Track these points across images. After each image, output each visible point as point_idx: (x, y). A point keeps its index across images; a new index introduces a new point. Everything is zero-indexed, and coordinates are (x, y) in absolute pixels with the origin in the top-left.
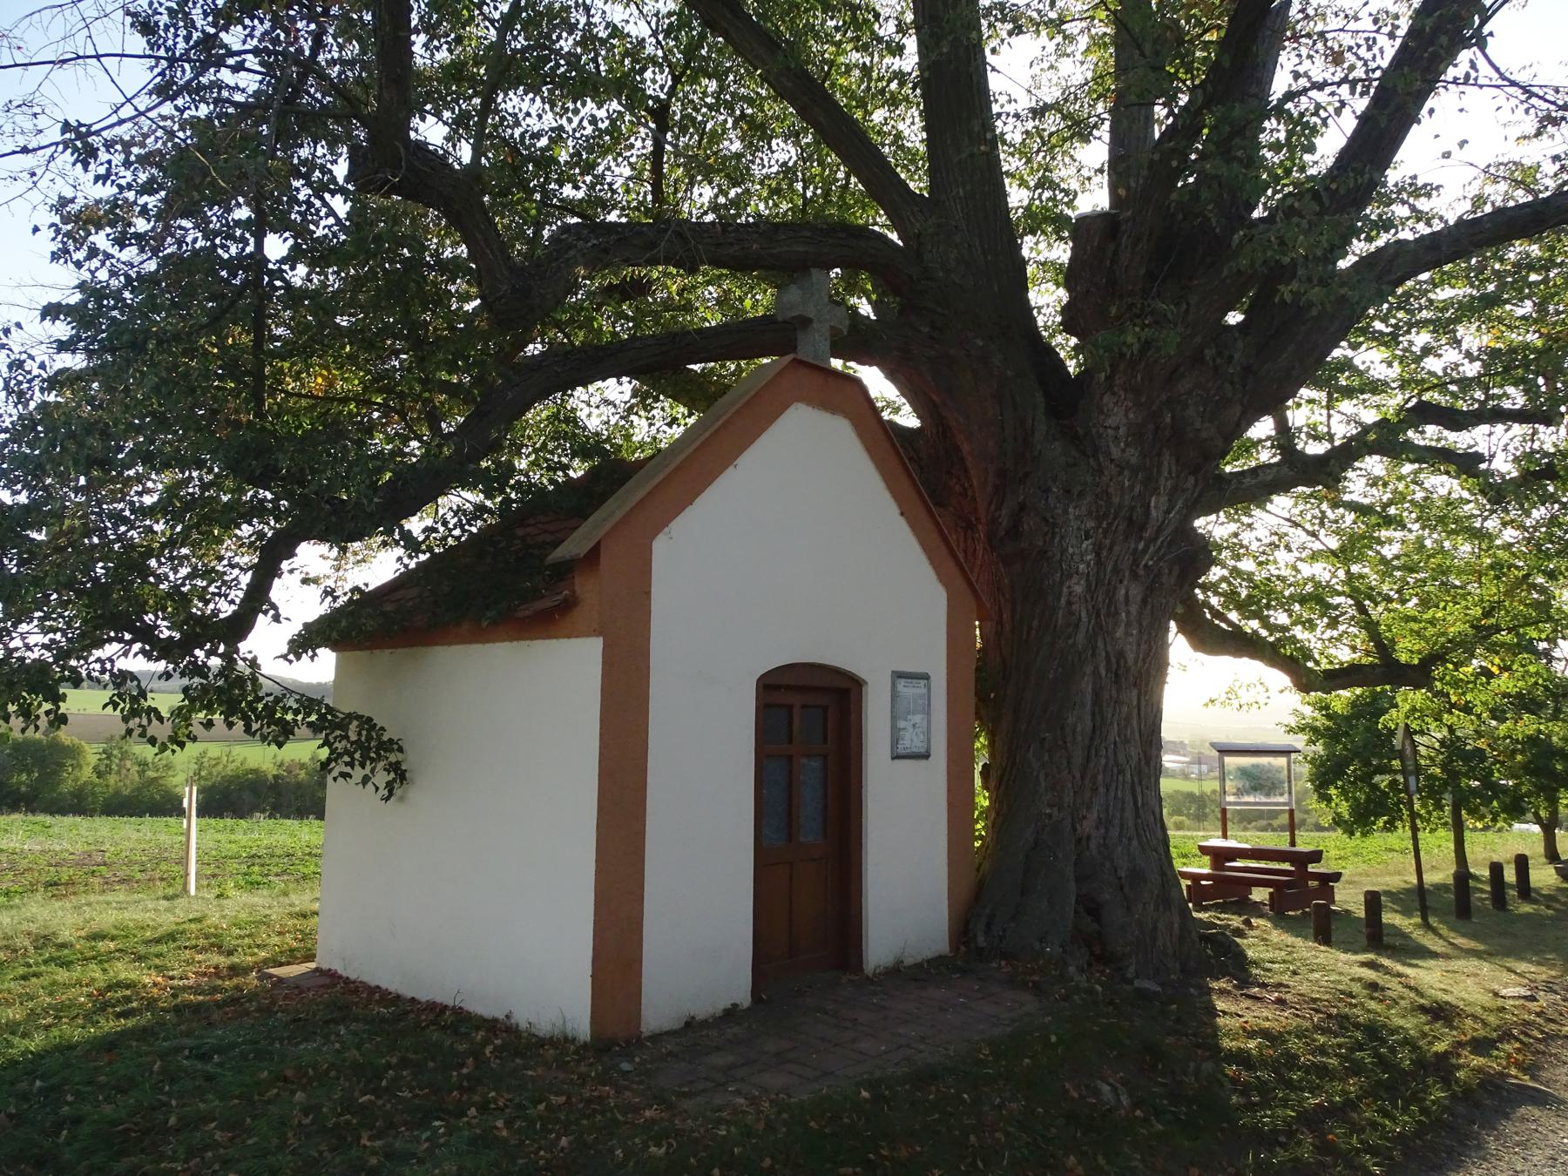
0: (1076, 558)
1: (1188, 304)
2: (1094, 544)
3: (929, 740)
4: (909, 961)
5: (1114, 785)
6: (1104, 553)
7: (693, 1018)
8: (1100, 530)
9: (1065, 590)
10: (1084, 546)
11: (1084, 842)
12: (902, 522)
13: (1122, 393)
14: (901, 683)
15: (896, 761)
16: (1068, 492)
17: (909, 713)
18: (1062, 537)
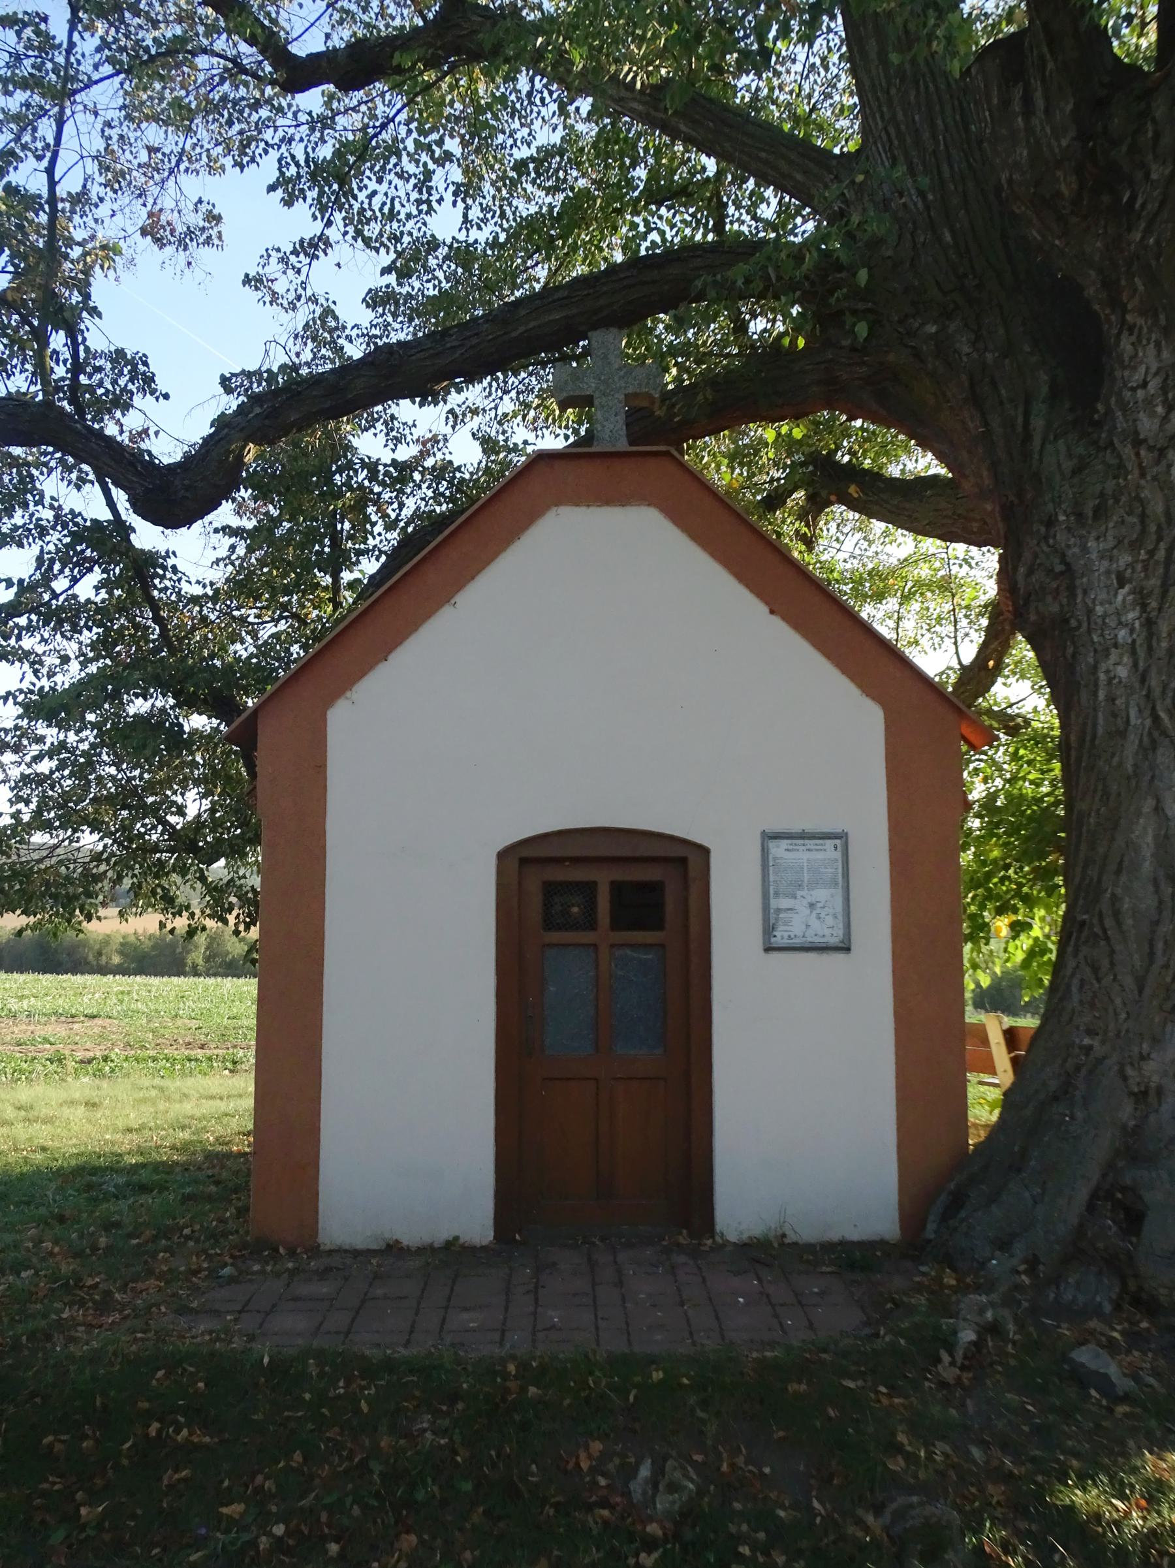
0: (1112, 622)
4: (791, 1238)
7: (397, 1241)
8: (1139, 567)
9: (1102, 676)
10: (1120, 598)
11: (1152, 1098)
12: (777, 622)
13: (1140, 321)
14: (779, 849)
15: (775, 955)
16: (1080, 516)
17: (800, 887)
18: (1085, 592)
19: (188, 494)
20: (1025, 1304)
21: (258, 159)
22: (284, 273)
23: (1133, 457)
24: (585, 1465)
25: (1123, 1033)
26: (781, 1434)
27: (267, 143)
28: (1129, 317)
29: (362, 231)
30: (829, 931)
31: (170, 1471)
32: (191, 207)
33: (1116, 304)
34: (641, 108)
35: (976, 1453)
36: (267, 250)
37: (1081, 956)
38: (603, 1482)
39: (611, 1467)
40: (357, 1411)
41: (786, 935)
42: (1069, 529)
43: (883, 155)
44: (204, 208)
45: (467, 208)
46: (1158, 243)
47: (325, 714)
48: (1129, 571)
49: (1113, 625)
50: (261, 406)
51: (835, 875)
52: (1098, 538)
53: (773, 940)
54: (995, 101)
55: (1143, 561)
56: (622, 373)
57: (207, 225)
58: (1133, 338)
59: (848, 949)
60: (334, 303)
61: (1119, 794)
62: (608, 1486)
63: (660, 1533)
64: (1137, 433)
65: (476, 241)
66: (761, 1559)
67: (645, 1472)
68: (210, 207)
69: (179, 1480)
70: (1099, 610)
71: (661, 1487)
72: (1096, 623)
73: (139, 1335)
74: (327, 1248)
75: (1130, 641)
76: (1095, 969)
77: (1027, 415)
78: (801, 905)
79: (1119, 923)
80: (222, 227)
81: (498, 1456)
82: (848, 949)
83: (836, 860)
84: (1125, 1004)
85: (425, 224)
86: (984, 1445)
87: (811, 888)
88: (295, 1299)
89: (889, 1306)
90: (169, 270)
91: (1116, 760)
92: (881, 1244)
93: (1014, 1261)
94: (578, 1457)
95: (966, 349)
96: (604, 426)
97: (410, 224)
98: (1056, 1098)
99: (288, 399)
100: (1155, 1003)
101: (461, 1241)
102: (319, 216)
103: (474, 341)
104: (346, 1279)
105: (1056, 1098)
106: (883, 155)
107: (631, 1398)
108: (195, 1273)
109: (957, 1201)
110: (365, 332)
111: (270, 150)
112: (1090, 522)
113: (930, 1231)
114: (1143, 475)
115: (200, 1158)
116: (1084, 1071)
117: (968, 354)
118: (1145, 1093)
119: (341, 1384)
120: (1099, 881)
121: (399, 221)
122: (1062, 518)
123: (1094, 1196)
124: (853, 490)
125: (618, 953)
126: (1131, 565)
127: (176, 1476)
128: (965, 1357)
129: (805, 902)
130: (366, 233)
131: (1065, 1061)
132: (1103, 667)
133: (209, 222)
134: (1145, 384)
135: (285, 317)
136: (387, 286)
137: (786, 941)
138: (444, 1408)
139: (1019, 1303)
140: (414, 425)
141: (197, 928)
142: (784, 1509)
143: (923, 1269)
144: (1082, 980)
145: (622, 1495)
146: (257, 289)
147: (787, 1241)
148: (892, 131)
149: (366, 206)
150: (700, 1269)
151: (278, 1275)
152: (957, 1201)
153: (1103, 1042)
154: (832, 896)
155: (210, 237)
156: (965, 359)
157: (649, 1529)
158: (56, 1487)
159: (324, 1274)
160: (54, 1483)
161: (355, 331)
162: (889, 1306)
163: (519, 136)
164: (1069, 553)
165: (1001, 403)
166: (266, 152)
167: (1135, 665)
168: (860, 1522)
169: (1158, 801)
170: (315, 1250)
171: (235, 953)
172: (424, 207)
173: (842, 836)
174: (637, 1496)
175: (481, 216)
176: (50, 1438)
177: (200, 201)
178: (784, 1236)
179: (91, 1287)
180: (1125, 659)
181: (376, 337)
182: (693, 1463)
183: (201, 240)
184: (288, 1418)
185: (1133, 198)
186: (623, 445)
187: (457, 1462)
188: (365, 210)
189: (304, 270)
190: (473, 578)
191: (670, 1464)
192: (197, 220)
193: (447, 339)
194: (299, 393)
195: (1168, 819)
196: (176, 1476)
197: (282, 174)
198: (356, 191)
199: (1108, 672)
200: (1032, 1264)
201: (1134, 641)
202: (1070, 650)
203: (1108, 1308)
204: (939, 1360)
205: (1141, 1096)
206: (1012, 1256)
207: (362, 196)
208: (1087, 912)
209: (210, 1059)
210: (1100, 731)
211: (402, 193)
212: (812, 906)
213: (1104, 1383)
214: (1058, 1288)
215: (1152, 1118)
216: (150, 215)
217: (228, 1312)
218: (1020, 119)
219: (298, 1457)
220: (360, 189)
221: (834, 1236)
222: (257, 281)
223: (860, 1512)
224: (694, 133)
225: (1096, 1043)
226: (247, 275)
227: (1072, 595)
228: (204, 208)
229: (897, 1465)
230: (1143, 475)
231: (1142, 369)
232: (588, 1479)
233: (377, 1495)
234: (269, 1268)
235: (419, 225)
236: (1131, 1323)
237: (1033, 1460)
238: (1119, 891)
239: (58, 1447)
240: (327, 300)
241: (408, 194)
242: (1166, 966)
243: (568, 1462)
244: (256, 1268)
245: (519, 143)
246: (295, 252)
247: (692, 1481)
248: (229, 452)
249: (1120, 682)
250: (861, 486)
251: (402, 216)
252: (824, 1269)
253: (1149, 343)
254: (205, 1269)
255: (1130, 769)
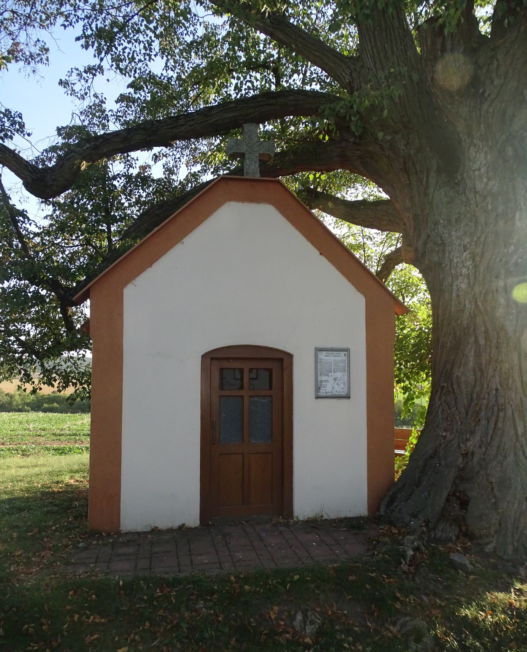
0: (460, 265)
1: (498, 60)
2: (470, 253)
3: (349, 388)
4: (325, 517)
5: (494, 418)
6: (478, 259)
7: (157, 527)
9: (455, 287)
10: (464, 256)
12: (323, 260)
13: (480, 143)
14: (322, 355)
16: (449, 221)
17: (330, 371)
18: (450, 252)
19: (53, 183)
20: (426, 539)
21: (73, 24)
22: (79, 81)
23: (474, 199)
24: (273, 616)
25: (459, 430)
26: (350, 597)
27: (78, 17)
28: (475, 141)
29: (119, 65)
30: (340, 389)
31: (89, 636)
32: (33, 43)
33: (470, 135)
34: (261, 24)
35: (425, 598)
36: (72, 69)
37: (443, 400)
38: (282, 623)
39: (284, 616)
40: (170, 602)
41: (324, 391)
42: (444, 227)
43: (370, 60)
44: (40, 44)
45: (168, 60)
46: (493, 111)
47: (122, 291)
48: (468, 245)
49: (460, 266)
50: (90, 144)
51: (345, 366)
52: (456, 231)
53: (319, 394)
54: (429, 43)
55: (475, 241)
56: (258, 144)
57: (41, 53)
58: (476, 150)
59: (348, 397)
60: (105, 99)
61: (460, 335)
62: (285, 624)
63: (310, 642)
64: (475, 188)
65: (172, 77)
66: (353, 648)
67: (299, 617)
68: (43, 44)
69: (94, 640)
70: (455, 260)
71: (308, 623)
72: (453, 266)
73: (53, 576)
74: (125, 531)
75: (467, 273)
76: (448, 405)
77: (428, 177)
78: (330, 379)
79: (459, 387)
80: (49, 55)
81: (236, 616)
82: (349, 397)
83: (345, 361)
84: (460, 419)
85: (147, 65)
86: (427, 595)
87: (335, 372)
88: (119, 555)
89: (374, 542)
90: (23, 73)
91: (459, 321)
92: (358, 519)
93: (420, 522)
94: (269, 614)
95: (403, 147)
96: (250, 167)
97: (140, 65)
98: (432, 457)
99: (103, 142)
100: (473, 418)
101: (186, 526)
102: (97, 55)
103: (191, 123)
104: (139, 545)
105: (432, 457)
106: (370, 60)
107: (288, 587)
108: (67, 546)
109: (392, 500)
110: (115, 114)
111: (80, 20)
112: (454, 224)
113: (382, 512)
114: (477, 206)
115: (39, 494)
116: (443, 446)
117: (403, 150)
118: (467, 454)
119: (158, 591)
120: (451, 369)
121: (135, 62)
122: (442, 222)
123: (449, 495)
124: (330, 204)
125: (252, 399)
126: (470, 243)
127: (92, 638)
128: (410, 561)
129: (332, 378)
130: (121, 66)
131: (435, 442)
132: (456, 284)
133: (42, 52)
134: (479, 169)
135: (78, 102)
136: (129, 93)
137: (324, 394)
138: (208, 598)
139: (423, 539)
140: (137, 160)
141: (37, 389)
142: (357, 627)
143: (381, 527)
144: (443, 410)
145: (291, 628)
146: (65, 87)
147: (323, 518)
148: (375, 50)
149: (121, 53)
150: (292, 532)
151: (105, 545)
152: (392, 500)
153: (451, 434)
154: (343, 375)
155: (41, 59)
156: (402, 152)
157: (306, 641)
158: (35, 648)
159: (128, 543)
160: (34, 647)
161: (110, 113)
162: (374, 542)
163: (189, 30)
164: (443, 236)
165: (416, 172)
166: (78, 21)
167: (469, 283)
168: (387, 629)
169: (476, 338)
170: (119, 534)
171: (4, 401)
172: (147, 58)
173: (347, 350)
174: (298, 628)
175: (173, 64)
176: (26, 626)
177: (38, 40)
178: (322, 516)
179: (18, 556)
180: (465, 281)
181: (120, 116)
182: (317, 612)
183: (37, 60)
184: (139, 608)
185: (484, 92)
186: (258, 176)
187: (219, 620)
188: (121, 55)
189: (90, 81)
190: (191, 232)
191: (309, 613)
192: (35, 50)
193: (179, 121)
194: (108, 139)
195: (480, 345)
196: (92, 638)
197: (84, 33)
198: (117, 46)
199: (457, 285)
200: (427, 522)
201: (469, 273)
202: (441, 276)
203: (454, 538)
204: (401, 563)
205: (465, 455)
206: (418, 520)
207: (120, 48)
208: (445, 382)
209: (9, 449)
210: (453, 309)
211: (138, 50)
212: (335, 379)
213: (463, 567)
214: (435, 532)
215: (470, 463)
216: (14, 44)
217: (91, 563)
218: (439, 52)
219: (147, 624)
220: (119, 45)
221: (342, 516)
222: (66, 83)
223: (387, 625)
224: (285, 39)
225: (448, 435)
226: (61, 80)
227: (444, 254)
228: (40, 44)
229: (398, 606)
230: (477, 206)
231: (479, 163)
232: (275, 622)
233: (187, 637)
234: (101, 542)
235: (144, 65)
236: (464, 544)
237: (447, 599)
238: (459, 374)
239: (31, 630)
240: (102, 96)
241: (140, 50)
242: (477, 404)
243: (266, 616)
244: (95, 542)
245: (189, 33)
246: (86, 72)
247: (319, 619)
248: (74, 165)
249: (462, 290)
250: (334, 203)
251: (137, 60)
252: (342, 529)
253: (482, 152)
254: (71, 544)
255: (465, 325)
